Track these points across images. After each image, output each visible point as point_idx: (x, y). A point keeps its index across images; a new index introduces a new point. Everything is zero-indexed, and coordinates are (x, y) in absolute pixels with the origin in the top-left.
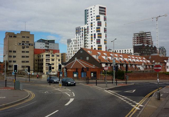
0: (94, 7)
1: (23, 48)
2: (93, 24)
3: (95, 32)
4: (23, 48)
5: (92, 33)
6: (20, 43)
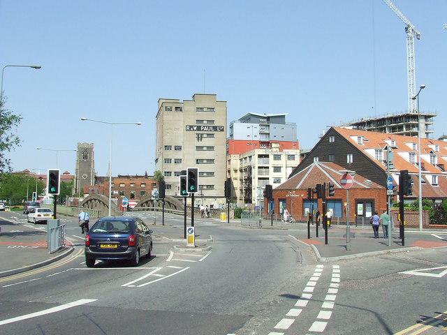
1: (200, 138)
4: (200, 138)
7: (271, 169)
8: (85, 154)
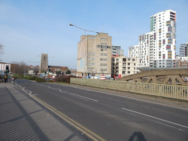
0: (163, 12)
1: (102, 50)
2: (162, 30)
3: (165, 38)
4: (102, 50)
5: (160, 39)
6: (99, 46)
7: (127, 68)
8: (45, 58)
